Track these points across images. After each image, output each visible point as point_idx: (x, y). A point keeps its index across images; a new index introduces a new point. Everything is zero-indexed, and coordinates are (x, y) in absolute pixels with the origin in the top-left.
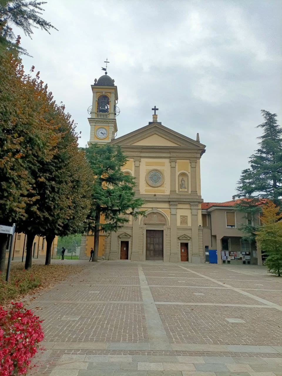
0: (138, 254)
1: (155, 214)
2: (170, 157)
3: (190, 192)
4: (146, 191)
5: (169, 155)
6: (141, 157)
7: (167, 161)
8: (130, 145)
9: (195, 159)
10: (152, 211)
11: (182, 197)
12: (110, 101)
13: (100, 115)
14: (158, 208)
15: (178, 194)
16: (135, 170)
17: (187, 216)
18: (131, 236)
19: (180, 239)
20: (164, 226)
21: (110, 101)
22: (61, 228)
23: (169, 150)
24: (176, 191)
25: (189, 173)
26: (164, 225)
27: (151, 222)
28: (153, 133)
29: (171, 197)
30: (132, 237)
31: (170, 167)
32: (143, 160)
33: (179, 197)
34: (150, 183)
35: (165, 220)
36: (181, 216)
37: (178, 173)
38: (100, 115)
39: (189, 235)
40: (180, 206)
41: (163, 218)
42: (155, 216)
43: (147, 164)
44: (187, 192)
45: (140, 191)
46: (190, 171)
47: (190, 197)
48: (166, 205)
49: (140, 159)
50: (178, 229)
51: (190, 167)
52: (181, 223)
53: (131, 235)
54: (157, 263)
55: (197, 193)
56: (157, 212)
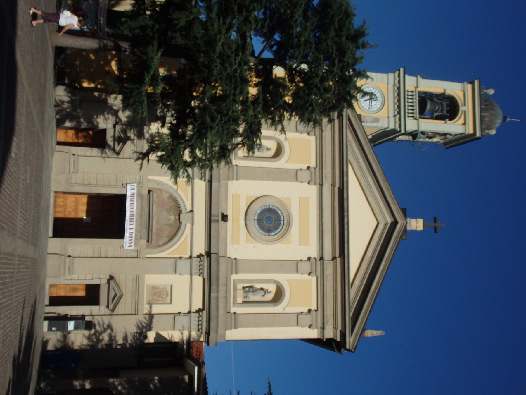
0: (72, 170)
1: (177, 217)
2: (322, 258)
3: (233, 310)
4: (237, 197)
5: (328, 256)
6: (321, 185)
7: (314, 253)
8: (348, 161)
9: (318, 181)
10: (183, 211)
11: (222, 288)
12: (445, 123)
13: (413, 113)
14: (192, 224)
15: (227, 279)
16: (287, 170)
17: (171, 303)
18: (113, 310)
19: (108, 282)
20: (144, 241)
21: (445, 123)
22: (139, 116)
23: (340, 256)
24: (236, 273)
25: (284, 309)
26: (148, 241)
27: (155, 206)
28: (379, 217)
29: (222, 260)
30: (111, 315)
31: (299, 259)
32: (314, 189)
33: (222, 280)
34: (257, 208)
35: (161, 243)
36: (171, 286)
37: (283, 278)
38: (413, 113)
39: (120, 309)
40: (198, 281)
41: (166, 239)
42: (172, 218)
43: (303, 202)
44: (235, 303)
45: (235, 181)
46: (289, 310)
47: (221, 311)
48: (200, 248)
49: (315, 184)
50: (138, 281)
51: (299, 168)
52: (154, 288)
53: (116, 312)
54: (54, 106)
55: (231, 329)
56: (180, 223)
